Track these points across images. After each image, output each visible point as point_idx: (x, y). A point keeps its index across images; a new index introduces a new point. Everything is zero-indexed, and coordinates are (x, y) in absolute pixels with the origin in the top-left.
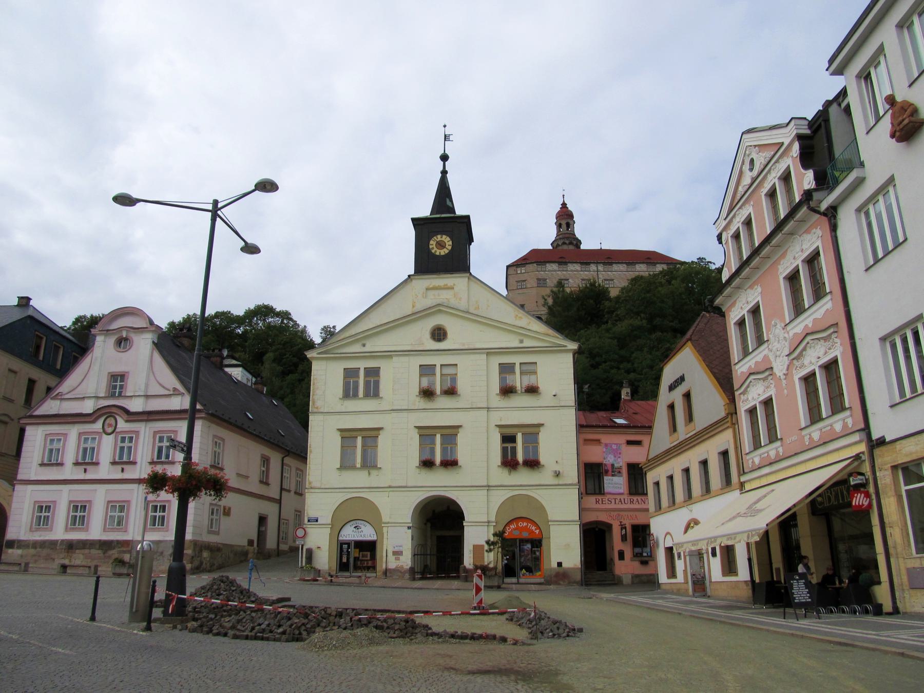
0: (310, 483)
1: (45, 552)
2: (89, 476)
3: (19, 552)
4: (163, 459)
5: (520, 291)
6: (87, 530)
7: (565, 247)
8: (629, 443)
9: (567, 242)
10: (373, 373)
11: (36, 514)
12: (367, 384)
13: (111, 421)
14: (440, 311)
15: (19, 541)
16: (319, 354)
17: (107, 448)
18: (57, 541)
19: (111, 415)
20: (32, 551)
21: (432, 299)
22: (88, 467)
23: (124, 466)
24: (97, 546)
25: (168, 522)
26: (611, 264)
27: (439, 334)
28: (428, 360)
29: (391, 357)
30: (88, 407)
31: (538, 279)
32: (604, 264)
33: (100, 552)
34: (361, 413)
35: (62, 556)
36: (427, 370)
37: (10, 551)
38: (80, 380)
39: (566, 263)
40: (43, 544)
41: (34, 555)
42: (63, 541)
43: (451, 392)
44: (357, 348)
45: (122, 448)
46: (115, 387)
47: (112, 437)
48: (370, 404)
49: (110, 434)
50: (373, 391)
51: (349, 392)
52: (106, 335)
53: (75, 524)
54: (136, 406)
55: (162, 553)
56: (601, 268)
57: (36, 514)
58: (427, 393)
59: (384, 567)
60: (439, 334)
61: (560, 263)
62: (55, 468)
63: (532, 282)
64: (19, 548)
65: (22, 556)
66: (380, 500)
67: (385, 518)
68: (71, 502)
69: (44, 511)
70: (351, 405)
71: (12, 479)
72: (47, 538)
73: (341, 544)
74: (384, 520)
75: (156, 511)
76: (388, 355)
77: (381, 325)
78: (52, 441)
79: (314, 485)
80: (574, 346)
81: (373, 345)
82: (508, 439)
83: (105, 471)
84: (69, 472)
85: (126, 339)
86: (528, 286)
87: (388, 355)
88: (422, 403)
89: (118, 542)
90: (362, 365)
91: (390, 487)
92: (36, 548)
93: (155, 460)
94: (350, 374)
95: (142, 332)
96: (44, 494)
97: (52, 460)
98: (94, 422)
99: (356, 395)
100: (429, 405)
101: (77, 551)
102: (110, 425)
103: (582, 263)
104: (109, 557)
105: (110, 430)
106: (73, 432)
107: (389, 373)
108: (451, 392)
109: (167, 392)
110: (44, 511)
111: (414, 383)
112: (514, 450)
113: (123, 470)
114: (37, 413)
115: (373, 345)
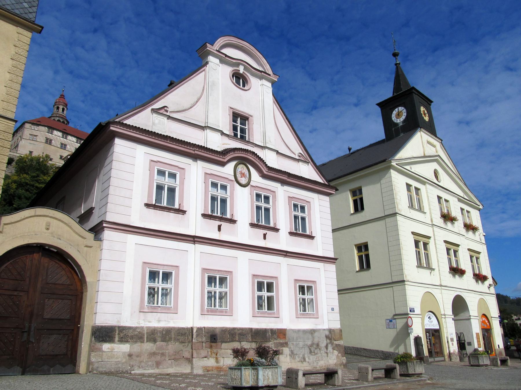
1: (172, 347)
3: (125, 348)
5: (32, 142)
6: (229, 313)
9: (61, 120)
11: (207, 289)
15: (122, 329)
17: (242, 204)
20: (148, 346)
35: (204, 353)
37: (106, 346)
39: (68, 134)
40: (167, 335)
41: (154, 354)
42: (199, 329)
47: (247, 189)
49: (244, 186)
55: (318, 345)
57: (207, 289)
59: (448, 352)
62: (172, 215)
63: (41, 138)
64: (123, 340)
65: (130, 355)
68: (204, 270)
69: (158, 281)
73: (426, 329)
75: (303, 294)
77: (194, 145)
86: (38, 140)
91: (441, 286)
92: (155, 341)
98: (223, 164)
101: (224, 345)
102: (243, 175)
110: (158, 281)
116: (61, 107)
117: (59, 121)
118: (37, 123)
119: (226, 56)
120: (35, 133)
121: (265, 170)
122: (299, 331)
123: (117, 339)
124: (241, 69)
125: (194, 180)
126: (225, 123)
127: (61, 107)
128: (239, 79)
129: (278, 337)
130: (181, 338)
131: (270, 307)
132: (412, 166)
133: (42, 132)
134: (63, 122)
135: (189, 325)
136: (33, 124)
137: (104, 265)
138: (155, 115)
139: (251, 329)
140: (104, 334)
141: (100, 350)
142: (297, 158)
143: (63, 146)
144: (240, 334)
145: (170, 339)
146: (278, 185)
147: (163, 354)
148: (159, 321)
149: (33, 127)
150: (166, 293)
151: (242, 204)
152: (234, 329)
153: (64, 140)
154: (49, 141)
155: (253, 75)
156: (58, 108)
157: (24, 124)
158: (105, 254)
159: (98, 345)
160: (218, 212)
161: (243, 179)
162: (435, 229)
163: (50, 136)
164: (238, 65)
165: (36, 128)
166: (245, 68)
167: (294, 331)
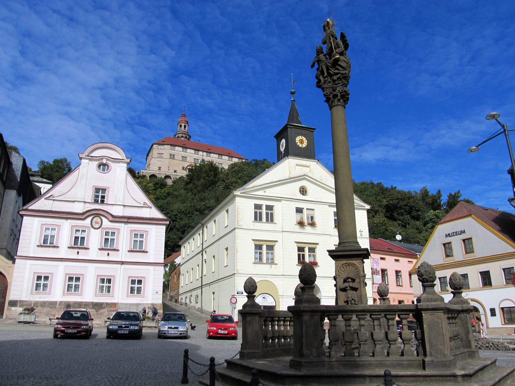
0: (237, 271)
2: (80, 257)
4: (79, 245)
7: (182, 139)
8: (382, 259)
9: (184, 136)
10: (270, 208)
12: (267, 214)
13: (97, 219)
14: (304, 179)
16: (241, 193)
17: (94, 239)
18: (56, 302)
19: (97, 215)
21: (298, 171)
22: (80, 251)
23: (110, 252)
24: (91, 306)
25: (113, 290)
26: (210, 153)
27: (303, 191)
28: (300, 205)
29: (280, 201)
30: (79, 208)
31: (171, 155)
32: (207, 152)
33: (93, 310)
34: (264, 231)
36: (299, 210)
37: (13, 308)
38: (69, 189)
39: (187, 148)
42: (61, 302)
43: (312, 224)
44: (261, 193)
45: (135, 241)
46: (97, 196)
48: (269, 226)
50: (270, 219)
51: (258, 217)
52: (90, 160)
53: (102, 292)
54: (117, 211)
56: (205, 154)
58: (301, 224)
60: (303, 191)
61: (183, 147)
66: (278, 282)
67: (280, 293)
68: (67, 274)
69: (42, 281)
70: (258, 225)
71: (11, 256)
72: (47, 300)
74: (280, 294)
75: (103, 282)
76: (278, 199)
78: (46, 229)
79: (240, 272)
80: (368, 207)
81: (270, 192)
82: (301, 249)
83: (93, 253)
84: (63, 252)
85: (104, 165)
86: (164, 157)
87: (278, 199)
88: (297, 228)
89: (107, 304)
90: (264, 203)
91: (283, 275)
93: (42, 244)
94: (258, 207)
95: (119, 162)
96: (43, 268)
97: (47, 242)
99: (261, 219)
100: (301, 230)
102: (97, 223)
103: (195, 150)
104: (101, 314)
105: (97, 226)
106: (66, 225)
107: (279, 209)
108: (312, 224)
109: (139, 205)
110: (42, 281)
111: (295, 217)
112: (303, 255)
113: (78, 253)
114: (31, 208)
115: (270, 192)
116: (183, 125)
117: (182, 137)
118: (161, 143)
119: (92, 157)
120: (161, 152)
121: (111, 218)
122: (127, 304)
123: (18, 305)
124: (104, 161)
125: (65, 230)
126: (89, 197)
127: (183, 125)
128: (103, 166)
129: (110, 307)
130: (52, 306)
131: (109, 291)
132: (267, 190)
133: (166, 149)
134: (186, 137)
135: (56, 300)
136: (159, 144)
137: (15, 275)
138: (46, 201)
139: (93, 303)
140: (13, 303)
141: (11, 310)
142: (142, 205)
143: (184, 158)
144: (85, 305)
145: (45, 306)
146: (122, 225)
147: (41, 313)
148: (40, 298)
149: (160, 147)
150: (45, 286)
151: (94, 239)
152: (82, 302)
153: (184, 154)
154: (172, 157)
155: (113, 162)
156: (181, 126)
157: (152, 145)
158: (16, 270)
159: (10, 308)
160: (79, 243)
161: (97, 225)
162: (284, 234)
163: (173, 152)
164: (102, 159)
165: (162, 147)
166: (107, 159)
167: (123, 304)
